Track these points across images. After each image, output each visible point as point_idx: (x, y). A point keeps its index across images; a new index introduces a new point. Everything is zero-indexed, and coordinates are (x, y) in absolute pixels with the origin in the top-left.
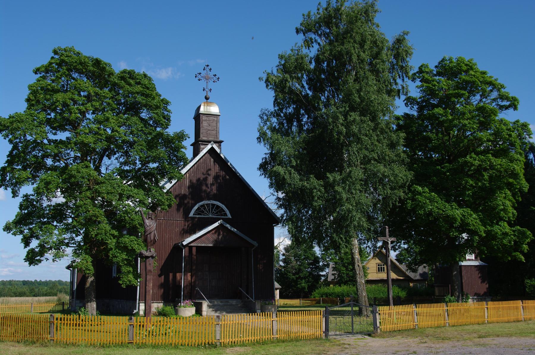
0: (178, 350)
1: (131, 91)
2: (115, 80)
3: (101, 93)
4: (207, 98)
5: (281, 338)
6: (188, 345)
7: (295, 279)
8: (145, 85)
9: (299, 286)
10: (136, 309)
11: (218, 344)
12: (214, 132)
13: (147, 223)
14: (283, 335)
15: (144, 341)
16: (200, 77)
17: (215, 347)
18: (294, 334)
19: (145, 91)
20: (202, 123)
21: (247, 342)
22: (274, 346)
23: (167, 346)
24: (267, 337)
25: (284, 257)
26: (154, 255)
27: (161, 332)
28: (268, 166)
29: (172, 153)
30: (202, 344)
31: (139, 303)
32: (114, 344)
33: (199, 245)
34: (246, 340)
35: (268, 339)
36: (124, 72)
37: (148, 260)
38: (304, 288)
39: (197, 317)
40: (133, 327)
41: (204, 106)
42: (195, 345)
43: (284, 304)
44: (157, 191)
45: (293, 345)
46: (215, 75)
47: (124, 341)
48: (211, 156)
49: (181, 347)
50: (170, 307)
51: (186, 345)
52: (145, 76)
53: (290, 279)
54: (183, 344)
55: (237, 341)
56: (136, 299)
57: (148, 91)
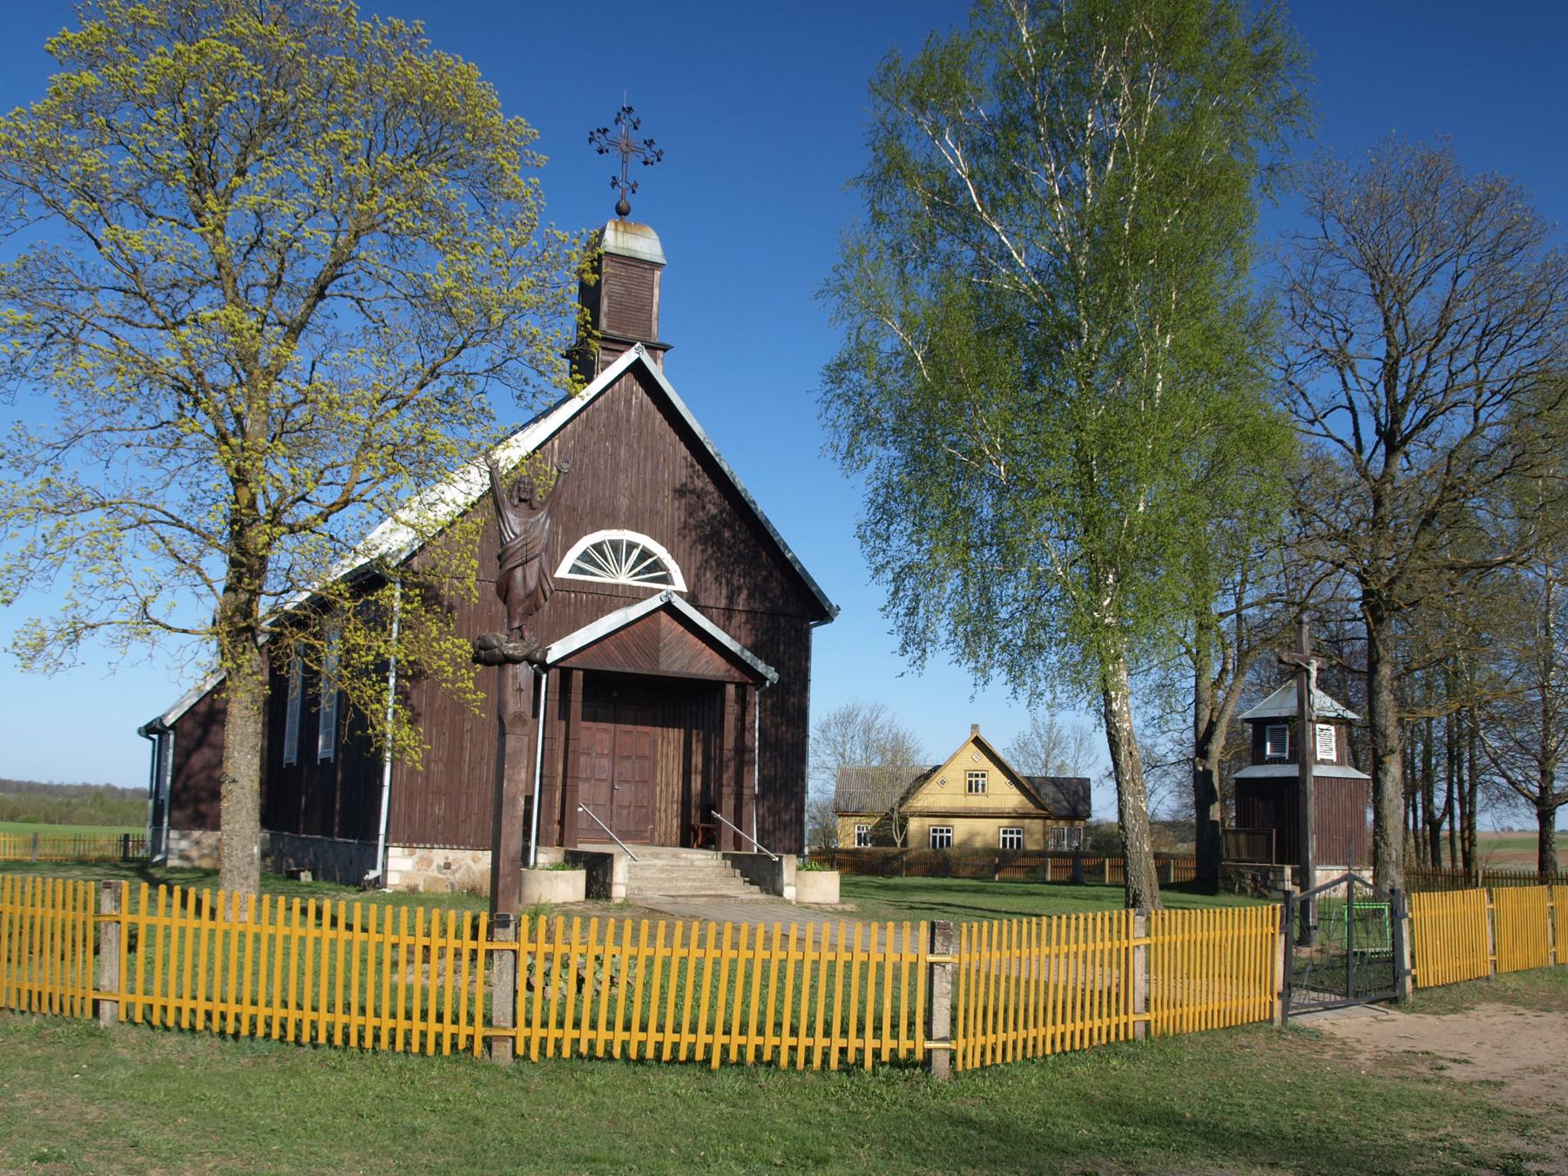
10: (374, 868)
31: (386, 848)
39: (597, 907)
41: (616, 230)
56: (378, 835)
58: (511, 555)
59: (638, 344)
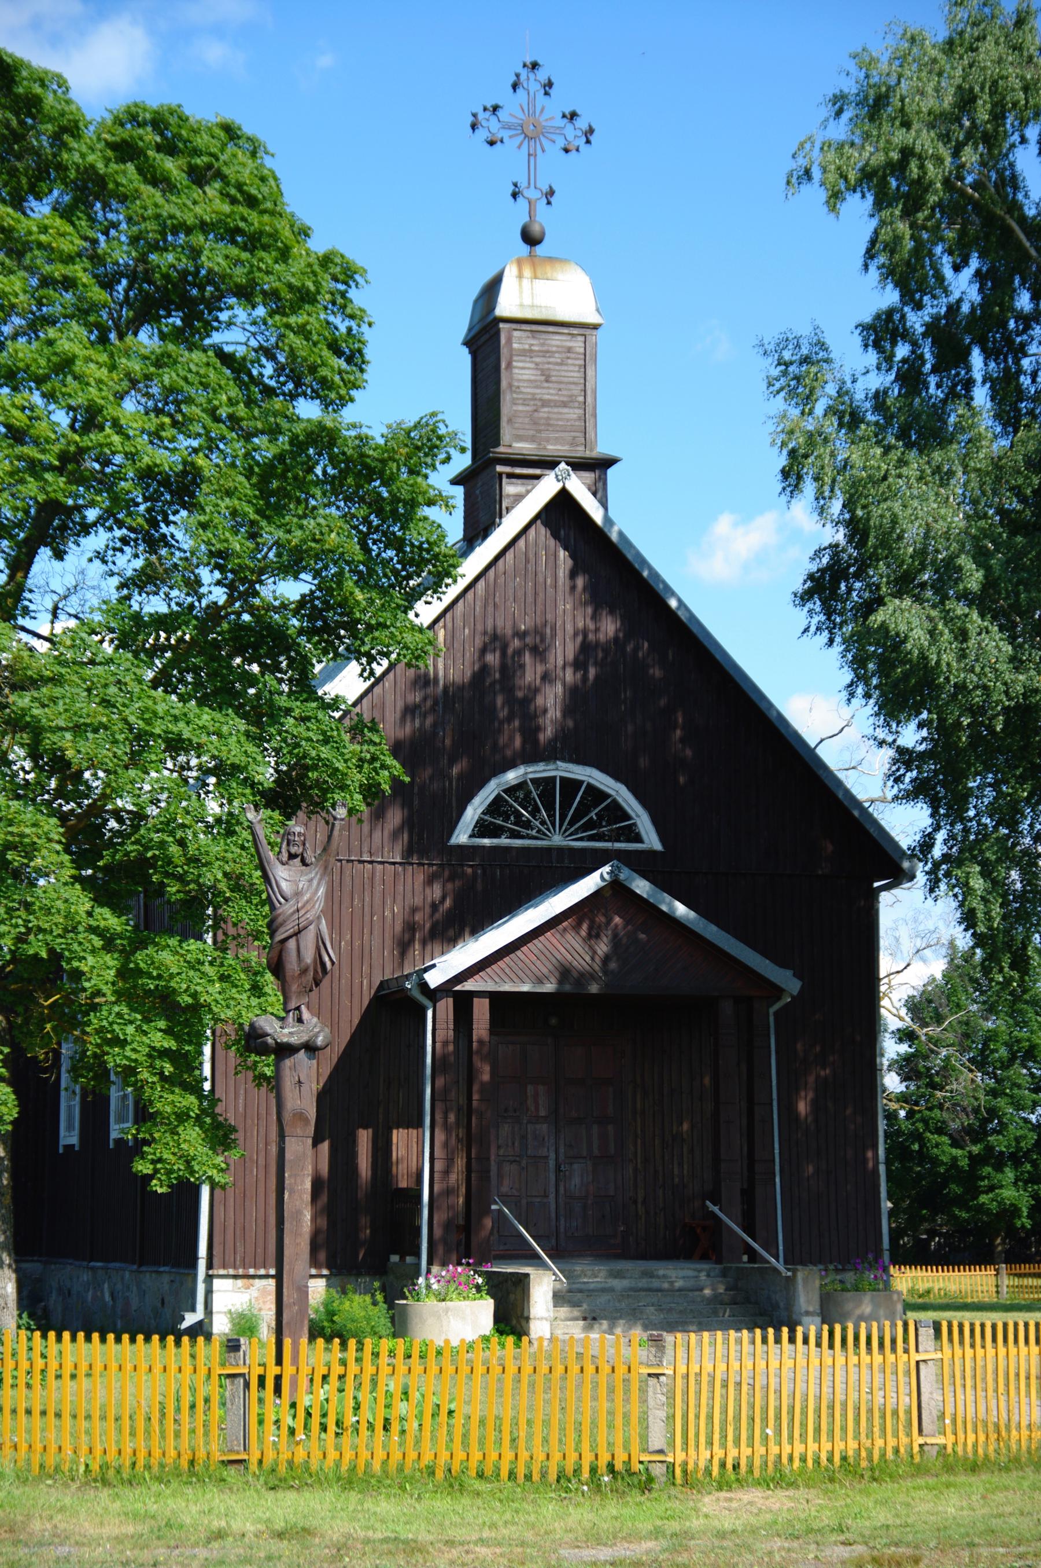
0: (466, 1501)
1: (172, 217)
2: (91, 158)
3: (30, 233)
4: (530, 238)
5: (960, 1449)
6: (512, 1476)
7: (964, 1163)
8: (239, 187)
9: (983, 1199)
10: (193, 1309)
11: (658, 1470)
12: (573, 413)
13: (284, 885)
14: (971, 1438)
15: (301, 1454)
16: (493, 124)
17: (646, 1484)
18: (1025, 1433)
19: (244, 219)
20: (509, 365)
21: (797, 1464)
22: (930, 1489)
23: (411, 1479)
24: (892, 1442)
25: (904, 1048)
26: (320, 1041)
27: (366, 1414)
28: (850, 590)
29: (377, 529)
30: (577, 1471)
31: (209, 1279)
32: (156, 1469)
33: (507, 987)
34: (791, 1459)
35: (897, 1451)
36: (132, 116)
37: (288, 1063)
38: (1014, 1211)
40: (247, 1385)
41: (520, 276)
42: (544, 1475)
43: (912, 1291)
44: (308, 719)
45: (1026, 1484)
46: (573, 116)
47: (201, 1454)
48: (555, 535)
49: (478, 1485)
50: (368, 1298)
51: (504, 1473)
52: (230, 131)
53: (935, 1161)
54: (488, 1473)
55: (751, 1460)
56: (195, 1258)
57: (253, 216)
58: (281, 925)
59: (563, 466)
